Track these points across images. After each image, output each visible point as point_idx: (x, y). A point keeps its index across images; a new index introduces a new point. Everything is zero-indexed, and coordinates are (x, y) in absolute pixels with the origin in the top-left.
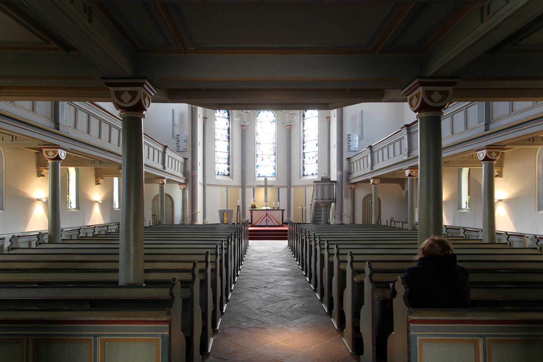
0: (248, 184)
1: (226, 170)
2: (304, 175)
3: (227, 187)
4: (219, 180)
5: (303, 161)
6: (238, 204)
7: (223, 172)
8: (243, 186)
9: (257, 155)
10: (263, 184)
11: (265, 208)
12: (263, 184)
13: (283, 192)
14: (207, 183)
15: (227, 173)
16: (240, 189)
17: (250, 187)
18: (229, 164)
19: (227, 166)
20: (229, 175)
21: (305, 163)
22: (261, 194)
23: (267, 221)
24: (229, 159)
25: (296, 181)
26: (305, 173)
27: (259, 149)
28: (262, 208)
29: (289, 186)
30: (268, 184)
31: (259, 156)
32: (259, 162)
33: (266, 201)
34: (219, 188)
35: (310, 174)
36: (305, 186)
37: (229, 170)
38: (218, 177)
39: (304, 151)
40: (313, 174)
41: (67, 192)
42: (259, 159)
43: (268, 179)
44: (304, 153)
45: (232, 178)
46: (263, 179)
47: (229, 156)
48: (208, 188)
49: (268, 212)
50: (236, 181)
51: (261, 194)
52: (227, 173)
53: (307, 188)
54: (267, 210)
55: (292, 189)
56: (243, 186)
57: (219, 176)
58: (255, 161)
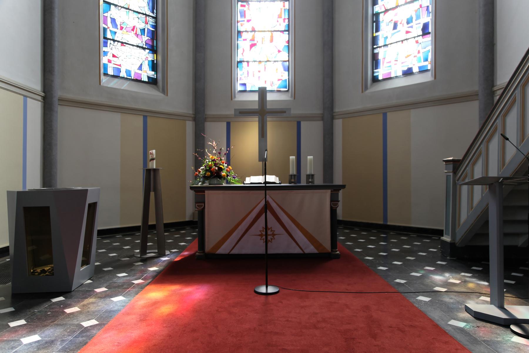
0: (211, 110)
1: (146, 67)
2: (375, 80)
3: (146, 114)
4: (112, 92)
5: (375, 40)
6: (153, 165)
7: (134, 70)
8: (199, 117)
9: (239, 33)
10: (256, 107)
11: (258, 179)
12: (256, 107)
13: (312, 132)
14: (59, 93)
15: (146, 73)
16: (190, 126)
17: (218, 118)
18: (153, 50)
19: (147, 56)
20: (152, 82)
21: (381, 42)
22: (248, 141)
23: (267, 235)
24: (154, 35)
25: (350, 99)
26: (381, 73)
27: (243, 14)
28: (250, 180)
29: (328, 115)
30: (269, 107)
31: (244, 35)
32: (243, 50)
33: (262, 159)
34: (117, 117)
35: (397, 71)
36: (384, 112)
37: (154, 66)
38: (114, 84)
39: (377, 9)
40: (408, 73)
41: (466, 160)
43: (270, 97)
44: (376, 15)
45: (164, 91)
46: (255, 97)
47: (155, 27)
48: (64, 116)
49: (271, 197)
50: (177, 99)
51: (468, 327)
52: (146, 73)
53: (389, 116)
54: (266, 187)
55: (338, 124)
56: (199, 117)
57: (116, 80)
58: (230, 48)
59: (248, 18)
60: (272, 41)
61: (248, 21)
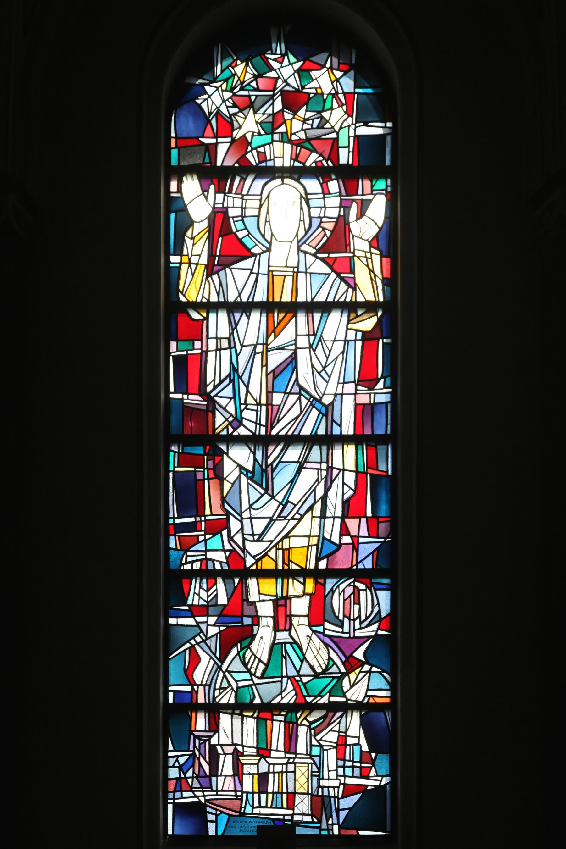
27: (192, 501)
42: (196, 626)
59: (212, 508)
60: (318, 614)
61: (218, 527)
